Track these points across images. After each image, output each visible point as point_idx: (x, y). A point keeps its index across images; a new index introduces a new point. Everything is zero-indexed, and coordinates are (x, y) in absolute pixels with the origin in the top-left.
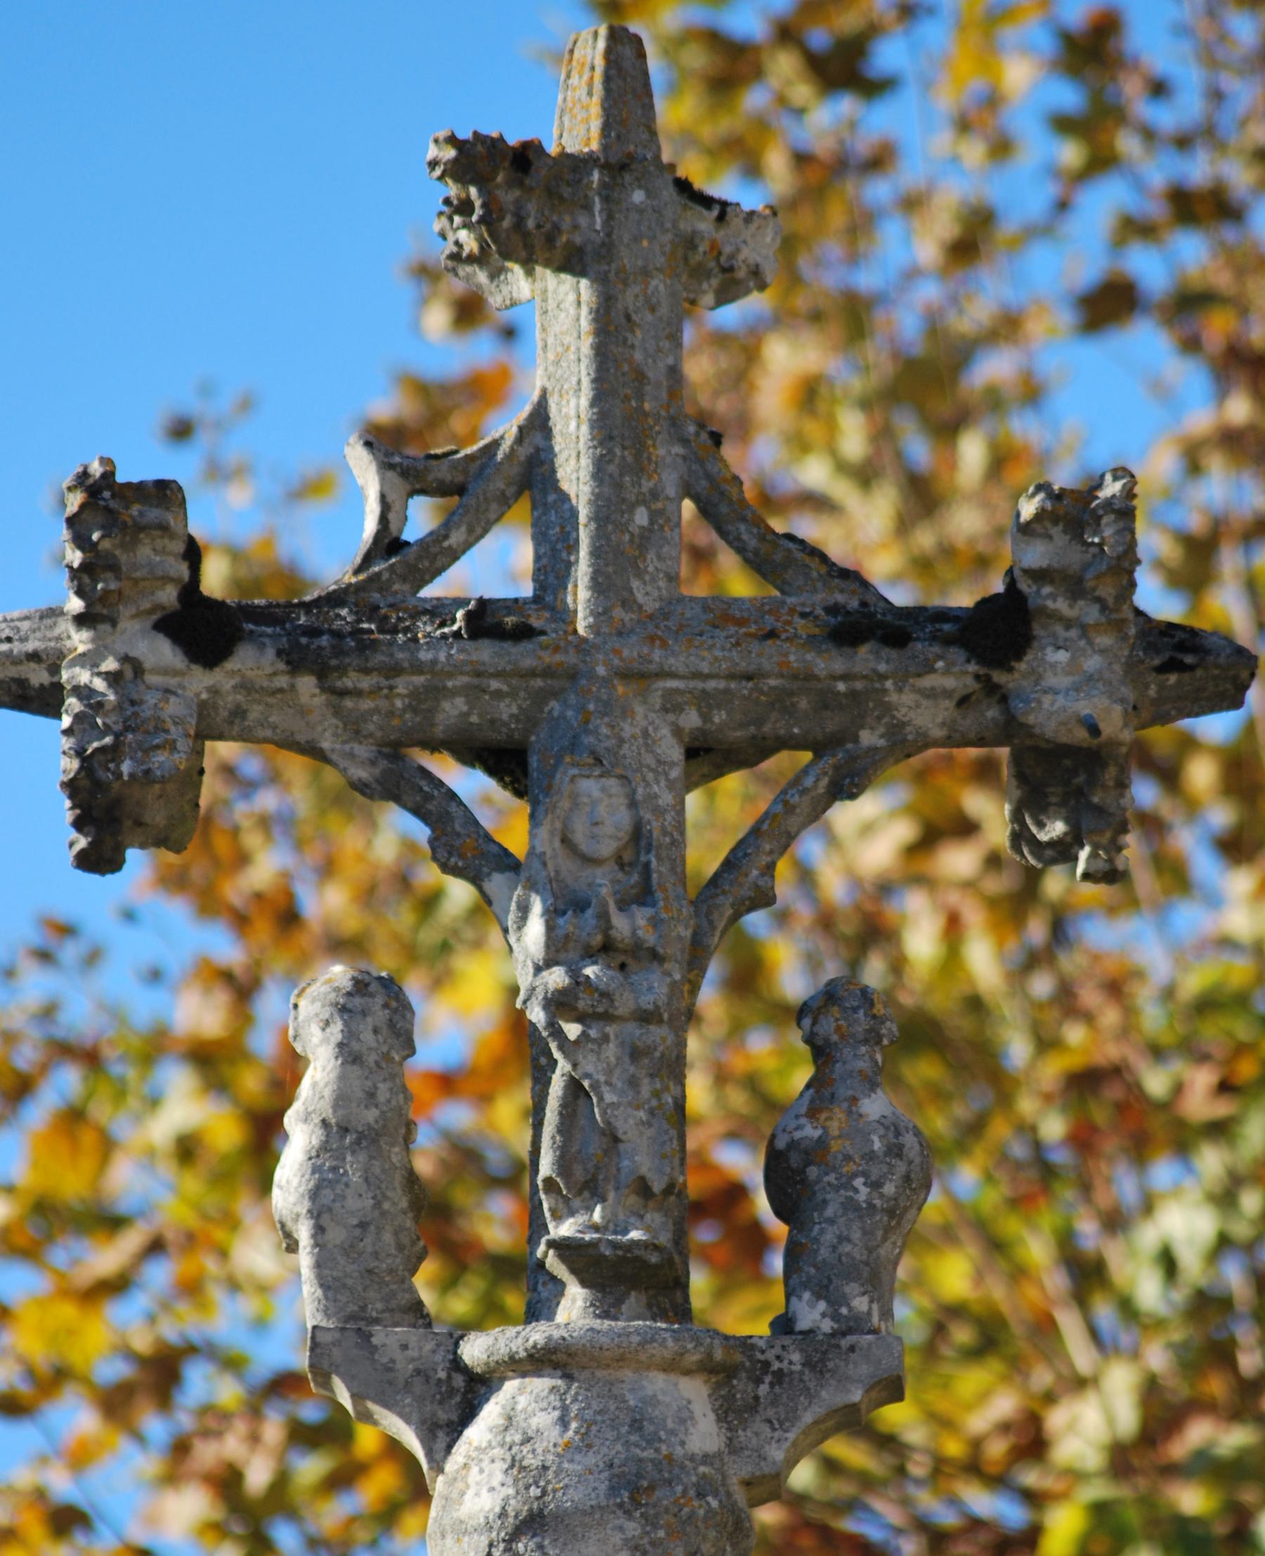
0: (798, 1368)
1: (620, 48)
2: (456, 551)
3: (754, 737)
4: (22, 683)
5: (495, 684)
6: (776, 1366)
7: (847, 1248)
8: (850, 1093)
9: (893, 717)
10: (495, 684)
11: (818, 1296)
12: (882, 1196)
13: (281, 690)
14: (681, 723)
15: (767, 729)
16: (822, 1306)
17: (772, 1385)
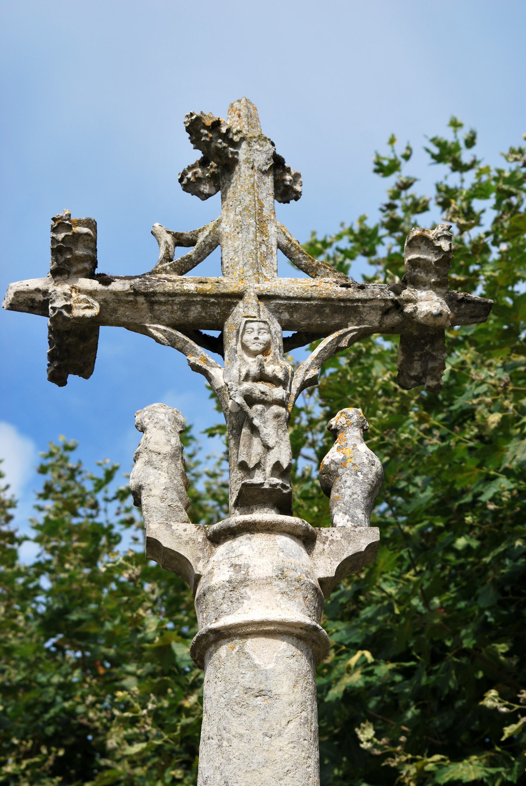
0: (339, 539)
1: (208, 310)
2: (193, 263)
3: (308, 324)
4: (33, 300)
5: (212, 300)
6: (330, 538)
7: (355, 496)
8: (353, 443)
9: (361, 317)
10: (212, 300)
11: (345, 514)
12: (368, 478)
13: (131, 301)
14: (282, 317)
15: (313, 321)
16: (347, 517)
17: (329, 545)
